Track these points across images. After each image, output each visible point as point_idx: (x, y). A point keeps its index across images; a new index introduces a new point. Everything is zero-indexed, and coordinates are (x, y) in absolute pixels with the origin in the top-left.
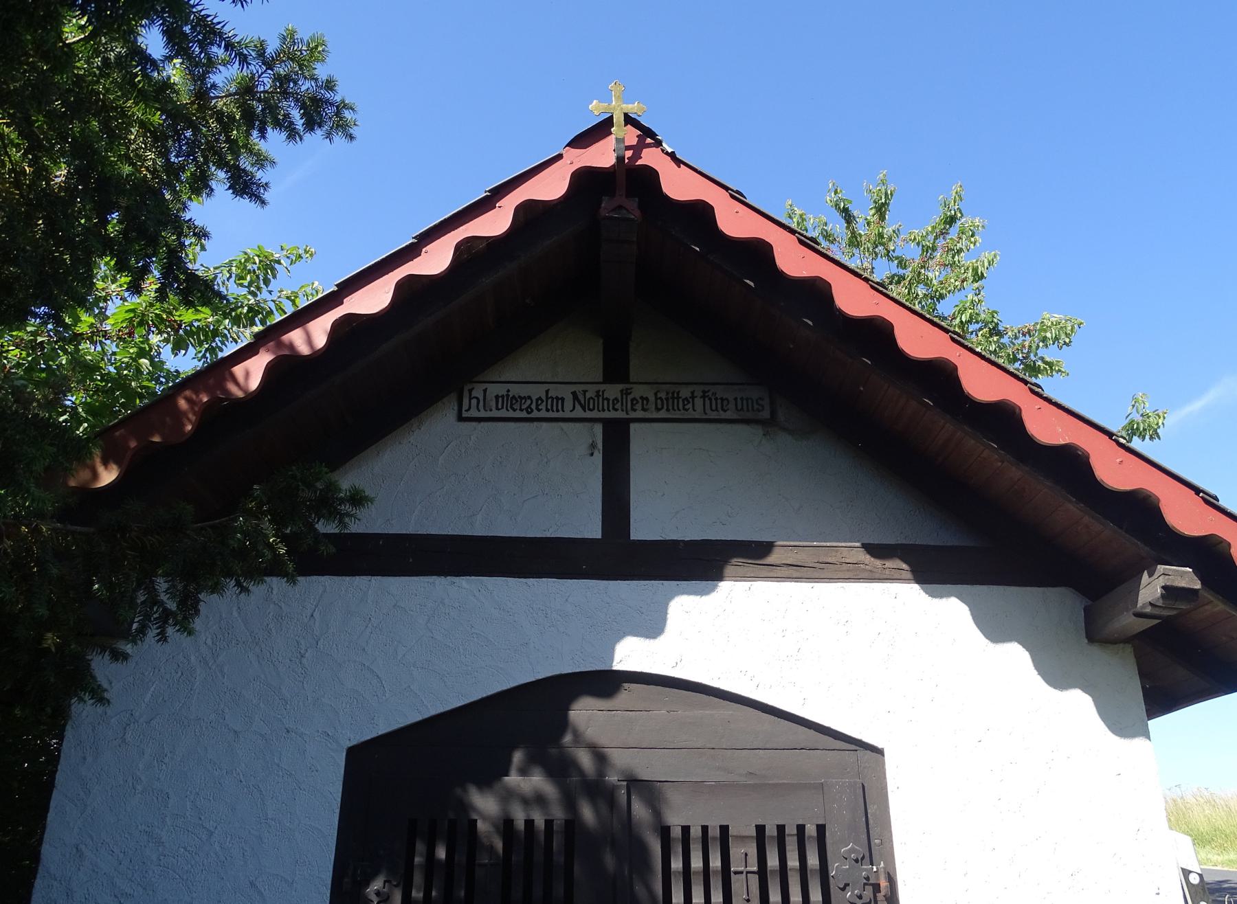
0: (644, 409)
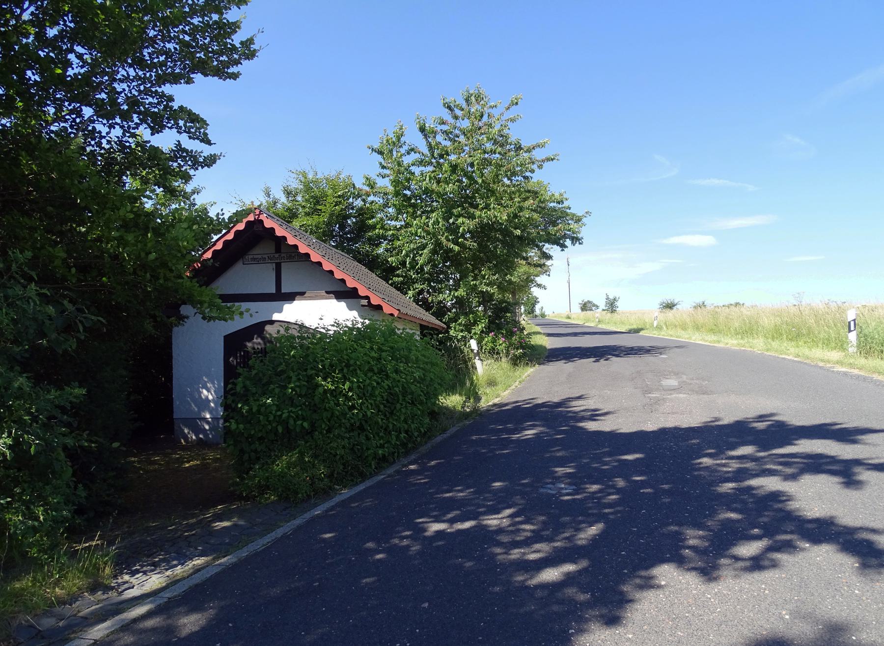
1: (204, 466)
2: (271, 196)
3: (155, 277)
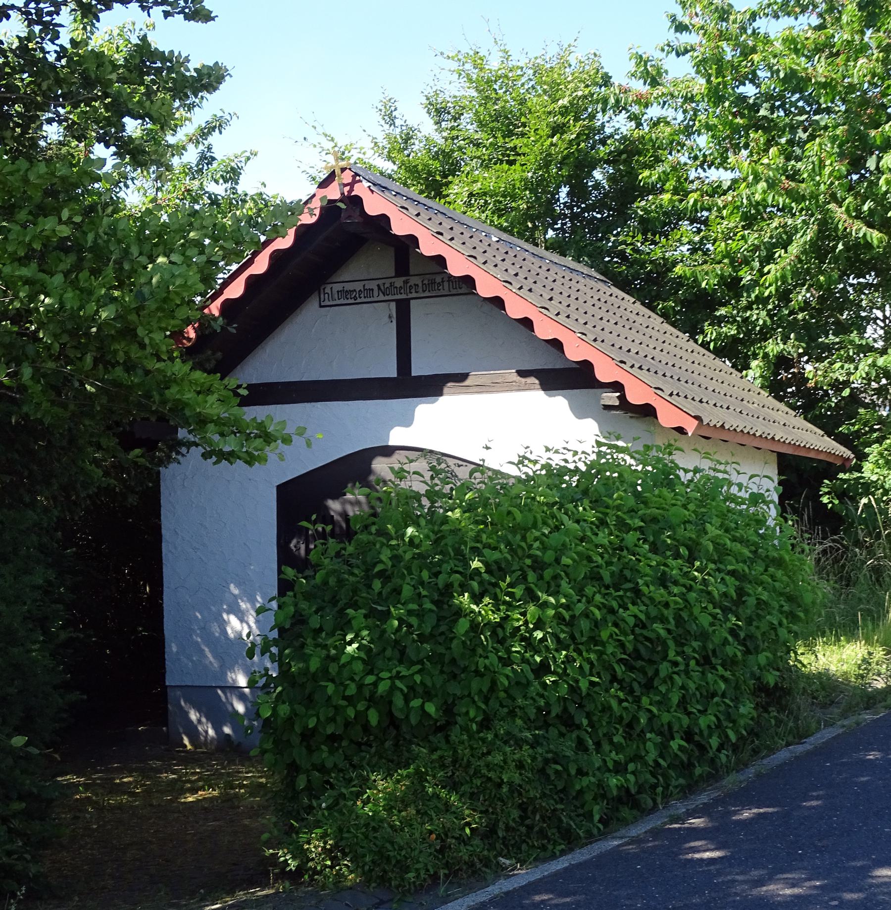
0: (416, 292)
1: (228, 801)
2: (398, 122)
3: (104, 360)
